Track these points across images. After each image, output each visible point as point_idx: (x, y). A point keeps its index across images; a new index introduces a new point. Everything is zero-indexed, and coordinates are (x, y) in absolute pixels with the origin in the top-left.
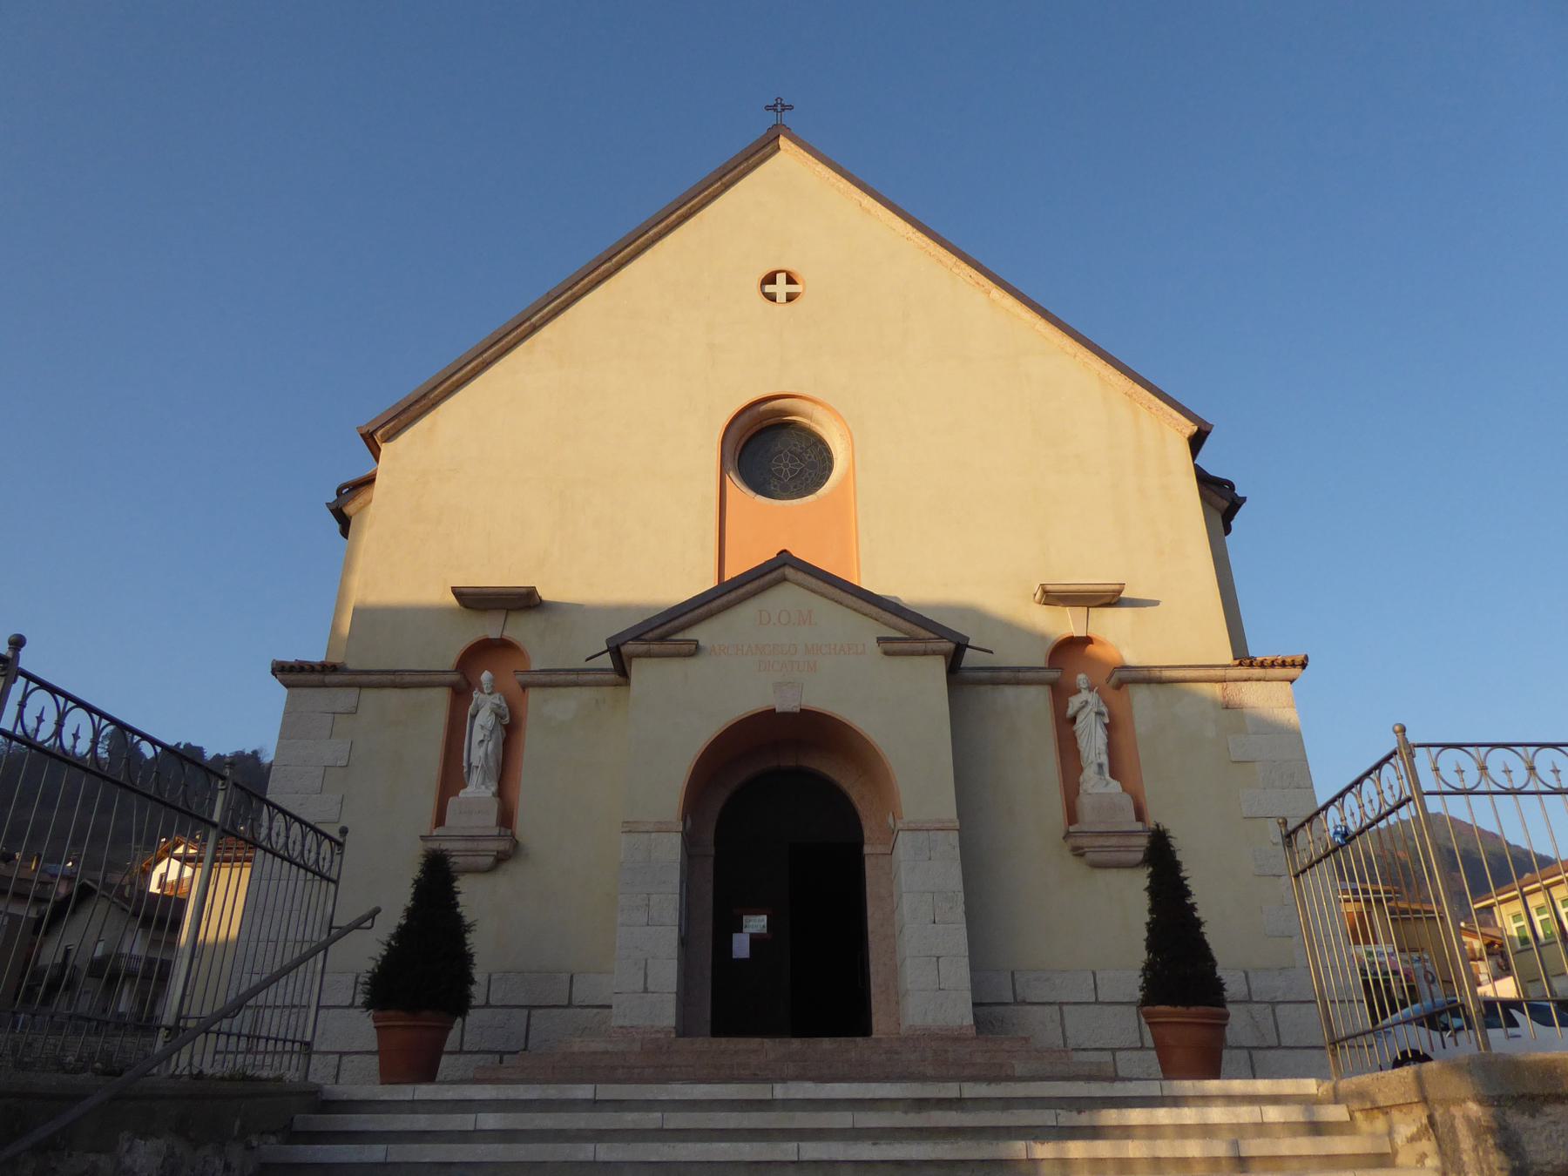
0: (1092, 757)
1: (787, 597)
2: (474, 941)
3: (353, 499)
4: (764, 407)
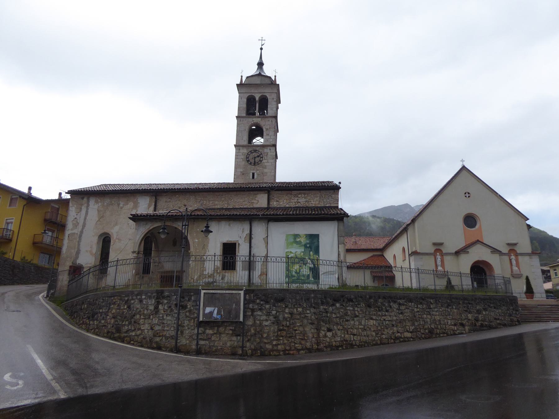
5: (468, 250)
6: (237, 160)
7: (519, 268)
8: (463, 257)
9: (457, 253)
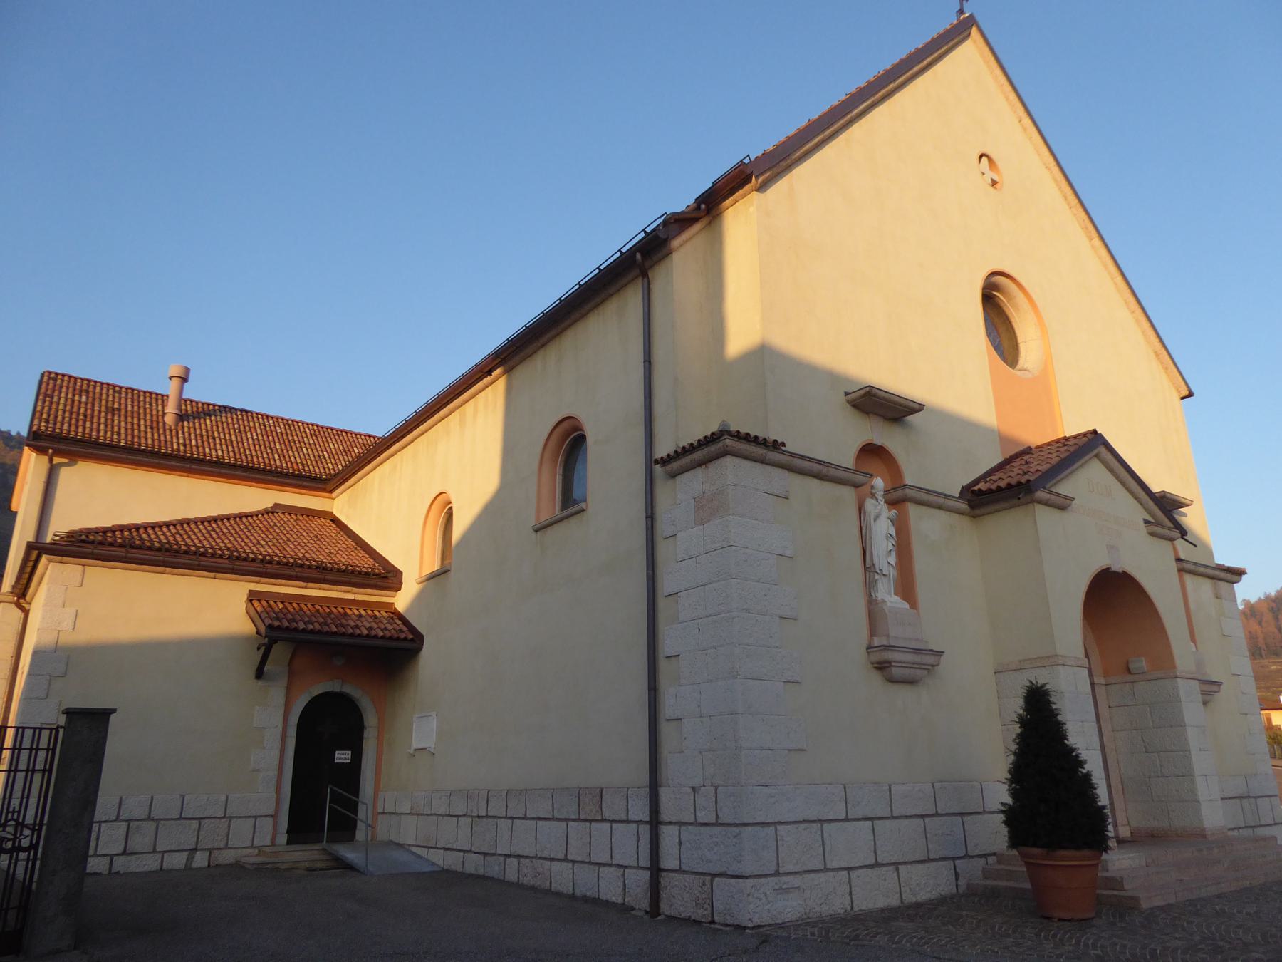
3: (679, 233)
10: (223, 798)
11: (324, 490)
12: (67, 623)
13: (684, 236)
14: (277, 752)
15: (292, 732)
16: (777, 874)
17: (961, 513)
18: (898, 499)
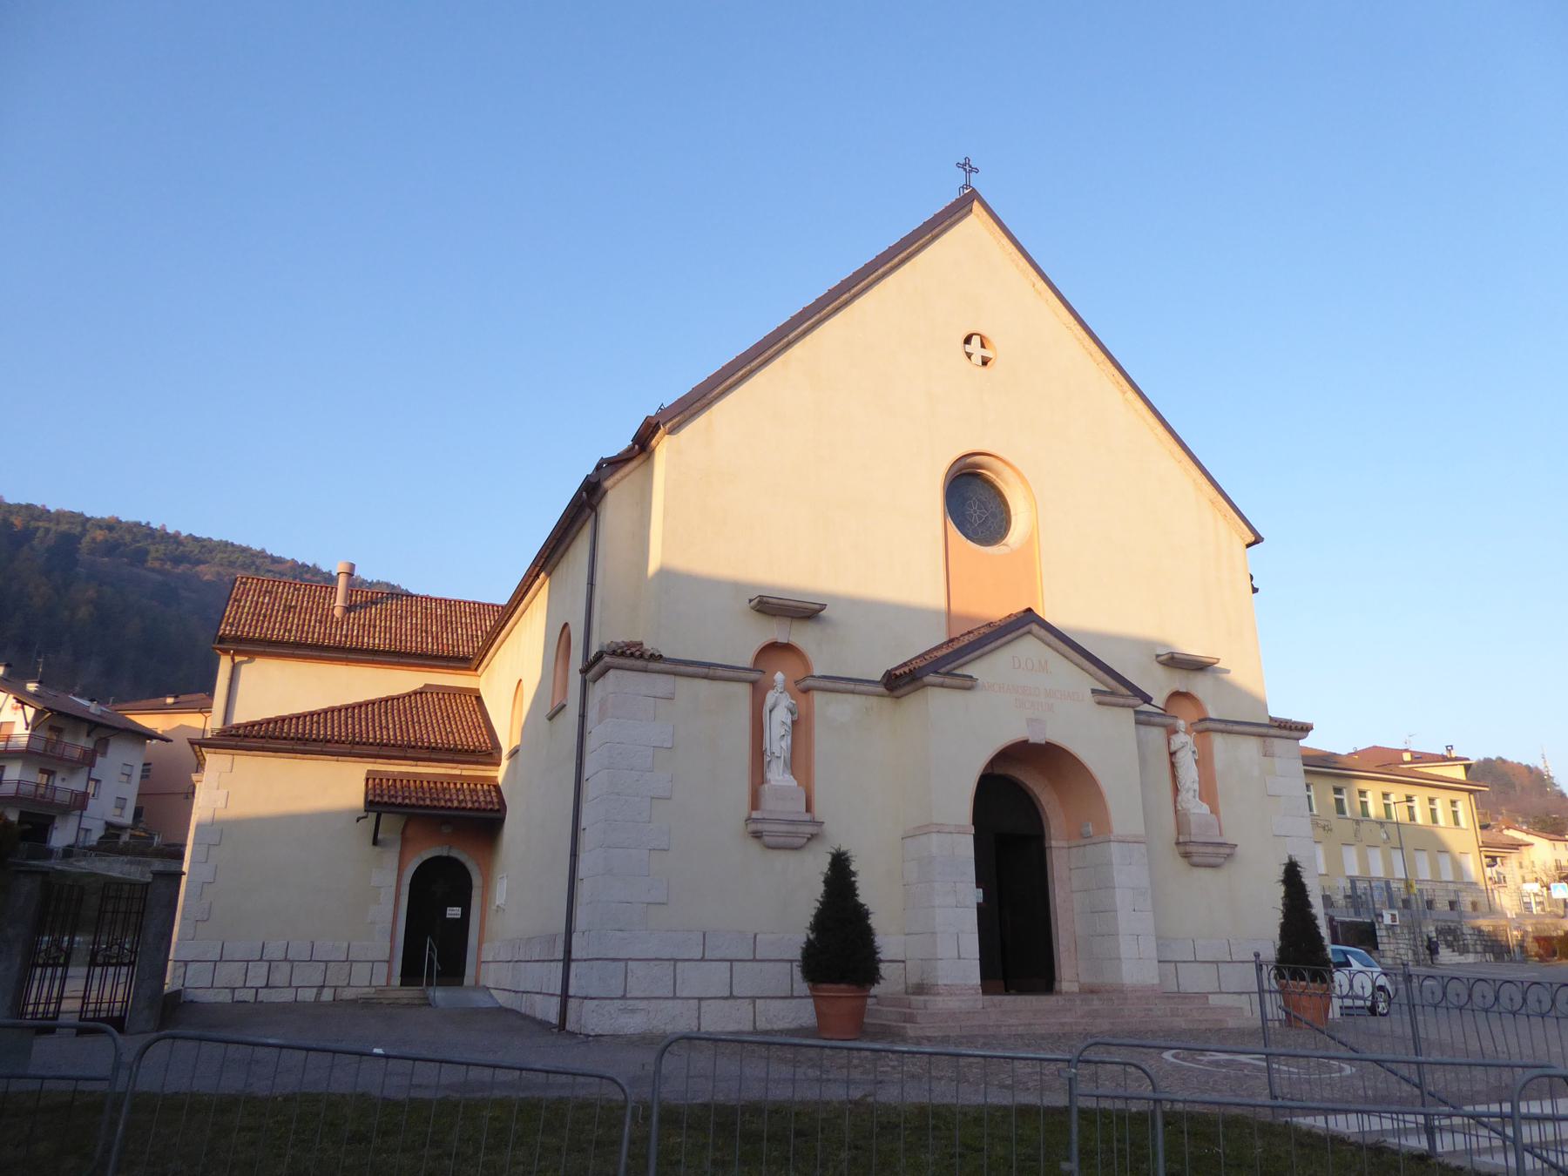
0: (1188, 784)
1: (1028, 648)
2: (873, 921)
3: (612, 474)
4: (970, 460)
5: (971, 670)
6: (126, 888)
7: (1214, 810)
8: (936, 702)
9: (899, 682)
10: (345, 945)
11: (468, 669)
12: (221, 803)
13: (617, 476)
14: (391, 907)
15: (405, 890)
16: (623, 997)
17: (882, 696)
18: (804, 688)
